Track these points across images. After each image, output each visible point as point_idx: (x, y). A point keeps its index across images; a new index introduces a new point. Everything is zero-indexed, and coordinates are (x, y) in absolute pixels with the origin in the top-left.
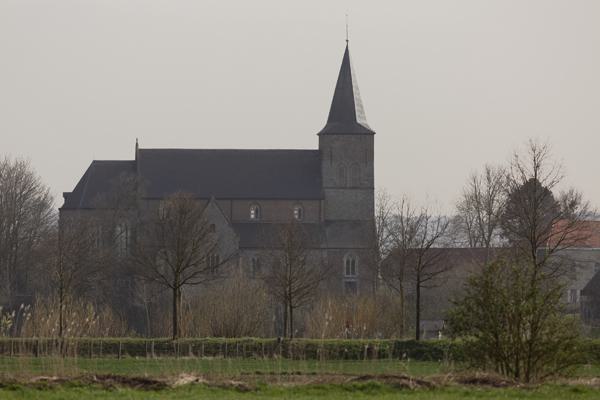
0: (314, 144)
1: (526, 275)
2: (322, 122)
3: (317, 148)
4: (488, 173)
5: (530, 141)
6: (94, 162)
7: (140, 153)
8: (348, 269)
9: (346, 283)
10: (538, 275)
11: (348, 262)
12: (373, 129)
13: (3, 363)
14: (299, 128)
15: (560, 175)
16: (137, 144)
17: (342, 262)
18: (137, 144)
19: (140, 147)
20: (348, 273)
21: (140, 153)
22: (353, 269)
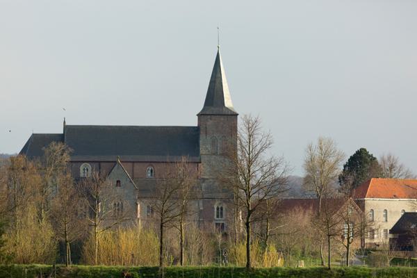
0: (194, 122)
1: (21, 222)
2: (199, 105)
3: (197, 125)
4: (321, 144)
5: (245, 116)
6: (33, 134)
7: (67, 128)
8: (218, 213)
9: (217, 224)
10: (164, 221)
11: (218, 209)
12: (238, 112)
13: (231, 277)
14: (184, 112)
15: (268, 142)
16: (65, 122)
17: (213, 208)
18: (65, 122)
19: (67, 124)
20: (218, 217)
21: (66, 128)
22: (222, 213)
